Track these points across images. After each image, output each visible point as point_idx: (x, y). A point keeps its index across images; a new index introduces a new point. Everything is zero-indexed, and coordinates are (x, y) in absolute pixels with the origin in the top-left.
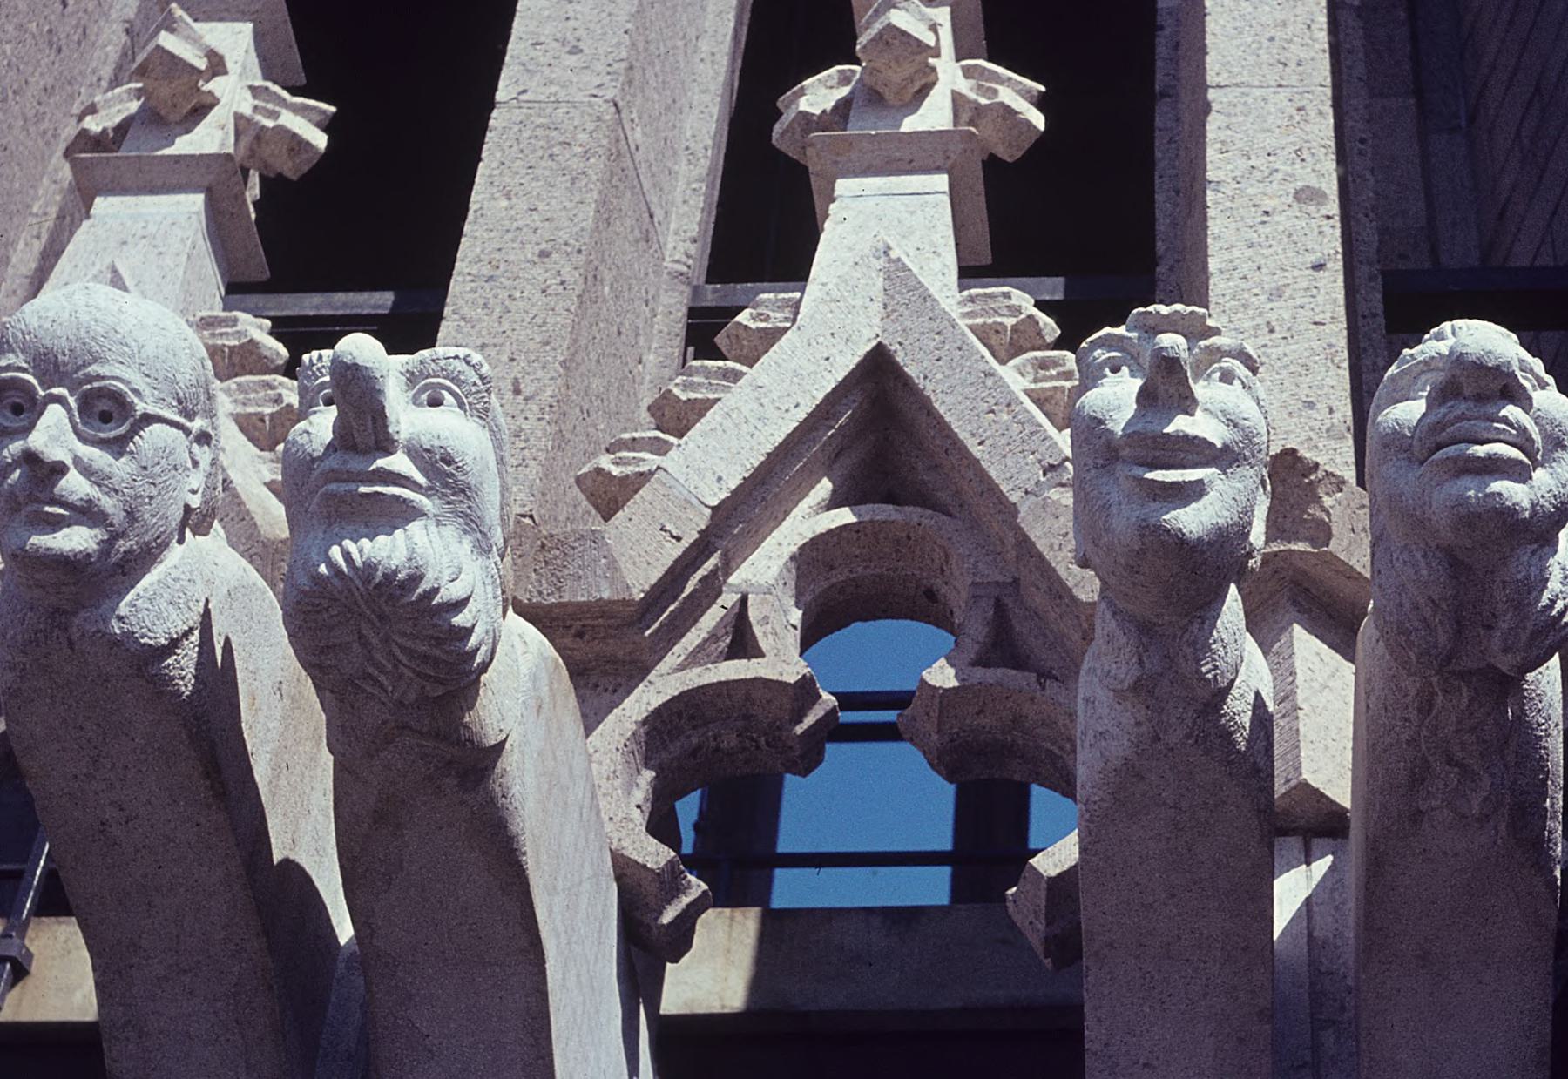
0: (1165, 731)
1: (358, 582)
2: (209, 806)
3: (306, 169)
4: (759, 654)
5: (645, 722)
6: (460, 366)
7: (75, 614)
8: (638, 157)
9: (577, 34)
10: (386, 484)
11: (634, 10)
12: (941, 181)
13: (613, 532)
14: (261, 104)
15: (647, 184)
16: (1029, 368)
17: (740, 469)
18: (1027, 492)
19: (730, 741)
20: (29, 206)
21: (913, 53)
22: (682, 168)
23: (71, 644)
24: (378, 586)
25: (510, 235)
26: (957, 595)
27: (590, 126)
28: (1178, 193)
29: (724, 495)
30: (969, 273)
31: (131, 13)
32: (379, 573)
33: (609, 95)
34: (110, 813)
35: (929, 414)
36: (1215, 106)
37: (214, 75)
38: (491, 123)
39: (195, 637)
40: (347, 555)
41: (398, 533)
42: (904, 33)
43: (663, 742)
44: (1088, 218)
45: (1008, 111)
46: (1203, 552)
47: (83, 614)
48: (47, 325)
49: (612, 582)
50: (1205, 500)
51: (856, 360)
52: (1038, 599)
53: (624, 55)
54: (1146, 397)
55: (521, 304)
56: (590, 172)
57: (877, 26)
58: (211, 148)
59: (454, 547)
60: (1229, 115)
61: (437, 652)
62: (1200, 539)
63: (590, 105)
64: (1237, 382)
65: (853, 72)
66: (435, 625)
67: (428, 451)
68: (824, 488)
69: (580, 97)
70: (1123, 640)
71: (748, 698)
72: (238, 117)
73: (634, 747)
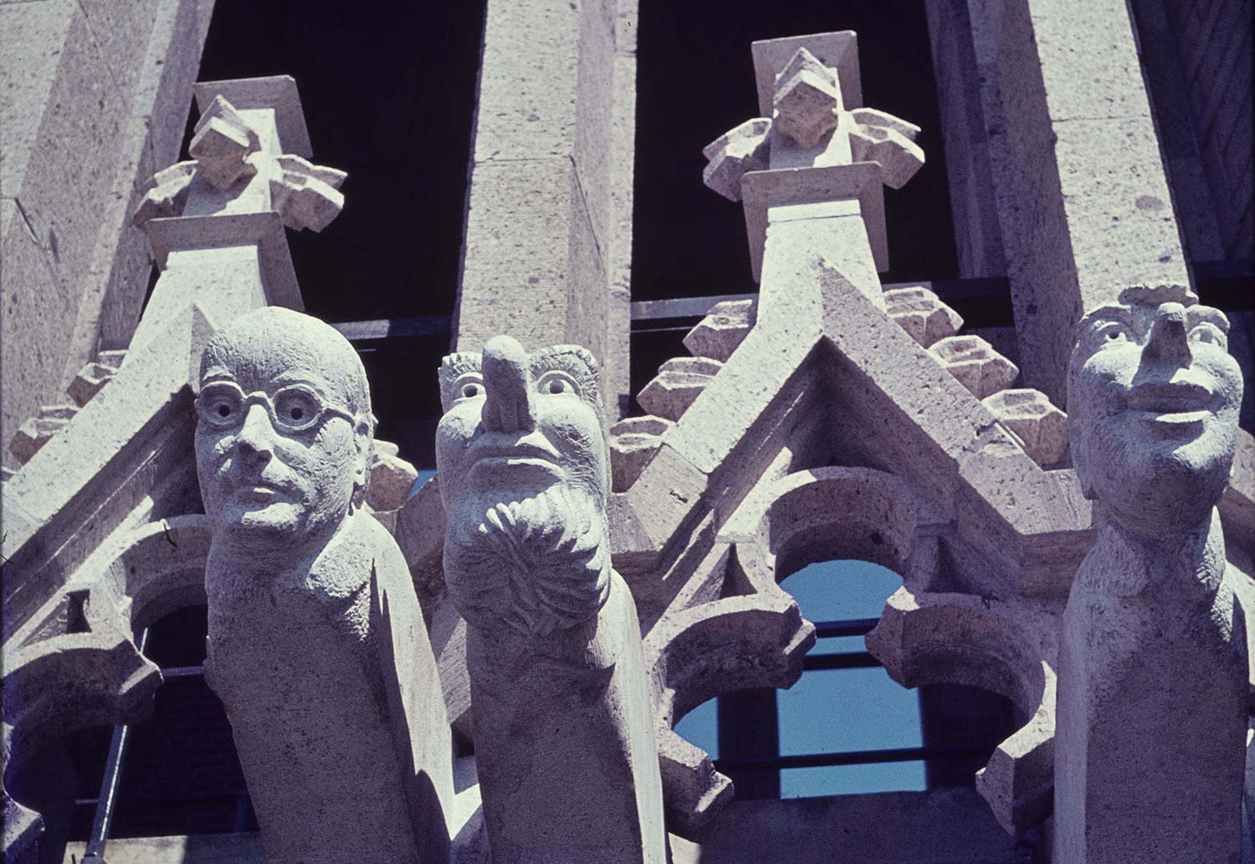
0: (1166, 629)
1: (512, 538)
2: (376, 728)
3: (328, 222)
4: (752, 591)
5: (666, 650)
6: (573, 359)
7: (276, 575)
8: (588, 202)
9: (533, 105)
10: (529, 456)
11: (575, 84)
12: (854, 206)
13: (634, 496)
14: (289, 173)
15: (594, 223)
16: (947, 351)
17: (727, 442)
18: (964, 449)
19: (731, 663)
20: (88, 267)
21: (822, 105)
22: (612, 209)
23: (273, 600)
24: (529, 539)
25: (503, 267)
26: (902, 536)
27: (555, 177)
28: (1017, 209)
29: (717, 463)
30: (887, 279)
31: (148, 110)
32: (529, 529)
33: (567, 151)
34: (295, 738)
35: (867, 392)
36: (1060, 136)
37: (252, 151)
38: (474, 178)
39: (367, 590)
40: (502, 516)
41: (540, 496)
42: (814, 89)
43: (679, 666)
44: (962, 236)
45: (897, 148)
46: (1203, 479)
47: (283, 575)
48: (245, 341)
49: (637, 538)
50: (1203, 437)
51: (807, 351)
52: (976, 536)
53: (573, 120)
54: (1150, 356)
55: (521, 321)
56: (560, 213)
57: (791, 85)
58: (258, 209)
59: (583, 506)
60: (1072, 143)
61: (573, 592)
62: (1202, 468)
63: (552, 161)
64: (1214, 341)
65: (766, 123)
66: (574, 570)
67: (559, 429)
68: (785, 456)
69: (543, 155)
70: (1132, 555)
71: (745, 626)
72: (273, 184)
73: (660, 671)
